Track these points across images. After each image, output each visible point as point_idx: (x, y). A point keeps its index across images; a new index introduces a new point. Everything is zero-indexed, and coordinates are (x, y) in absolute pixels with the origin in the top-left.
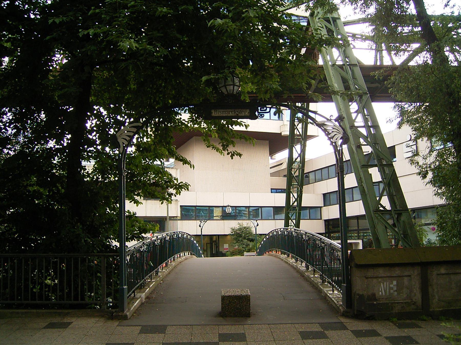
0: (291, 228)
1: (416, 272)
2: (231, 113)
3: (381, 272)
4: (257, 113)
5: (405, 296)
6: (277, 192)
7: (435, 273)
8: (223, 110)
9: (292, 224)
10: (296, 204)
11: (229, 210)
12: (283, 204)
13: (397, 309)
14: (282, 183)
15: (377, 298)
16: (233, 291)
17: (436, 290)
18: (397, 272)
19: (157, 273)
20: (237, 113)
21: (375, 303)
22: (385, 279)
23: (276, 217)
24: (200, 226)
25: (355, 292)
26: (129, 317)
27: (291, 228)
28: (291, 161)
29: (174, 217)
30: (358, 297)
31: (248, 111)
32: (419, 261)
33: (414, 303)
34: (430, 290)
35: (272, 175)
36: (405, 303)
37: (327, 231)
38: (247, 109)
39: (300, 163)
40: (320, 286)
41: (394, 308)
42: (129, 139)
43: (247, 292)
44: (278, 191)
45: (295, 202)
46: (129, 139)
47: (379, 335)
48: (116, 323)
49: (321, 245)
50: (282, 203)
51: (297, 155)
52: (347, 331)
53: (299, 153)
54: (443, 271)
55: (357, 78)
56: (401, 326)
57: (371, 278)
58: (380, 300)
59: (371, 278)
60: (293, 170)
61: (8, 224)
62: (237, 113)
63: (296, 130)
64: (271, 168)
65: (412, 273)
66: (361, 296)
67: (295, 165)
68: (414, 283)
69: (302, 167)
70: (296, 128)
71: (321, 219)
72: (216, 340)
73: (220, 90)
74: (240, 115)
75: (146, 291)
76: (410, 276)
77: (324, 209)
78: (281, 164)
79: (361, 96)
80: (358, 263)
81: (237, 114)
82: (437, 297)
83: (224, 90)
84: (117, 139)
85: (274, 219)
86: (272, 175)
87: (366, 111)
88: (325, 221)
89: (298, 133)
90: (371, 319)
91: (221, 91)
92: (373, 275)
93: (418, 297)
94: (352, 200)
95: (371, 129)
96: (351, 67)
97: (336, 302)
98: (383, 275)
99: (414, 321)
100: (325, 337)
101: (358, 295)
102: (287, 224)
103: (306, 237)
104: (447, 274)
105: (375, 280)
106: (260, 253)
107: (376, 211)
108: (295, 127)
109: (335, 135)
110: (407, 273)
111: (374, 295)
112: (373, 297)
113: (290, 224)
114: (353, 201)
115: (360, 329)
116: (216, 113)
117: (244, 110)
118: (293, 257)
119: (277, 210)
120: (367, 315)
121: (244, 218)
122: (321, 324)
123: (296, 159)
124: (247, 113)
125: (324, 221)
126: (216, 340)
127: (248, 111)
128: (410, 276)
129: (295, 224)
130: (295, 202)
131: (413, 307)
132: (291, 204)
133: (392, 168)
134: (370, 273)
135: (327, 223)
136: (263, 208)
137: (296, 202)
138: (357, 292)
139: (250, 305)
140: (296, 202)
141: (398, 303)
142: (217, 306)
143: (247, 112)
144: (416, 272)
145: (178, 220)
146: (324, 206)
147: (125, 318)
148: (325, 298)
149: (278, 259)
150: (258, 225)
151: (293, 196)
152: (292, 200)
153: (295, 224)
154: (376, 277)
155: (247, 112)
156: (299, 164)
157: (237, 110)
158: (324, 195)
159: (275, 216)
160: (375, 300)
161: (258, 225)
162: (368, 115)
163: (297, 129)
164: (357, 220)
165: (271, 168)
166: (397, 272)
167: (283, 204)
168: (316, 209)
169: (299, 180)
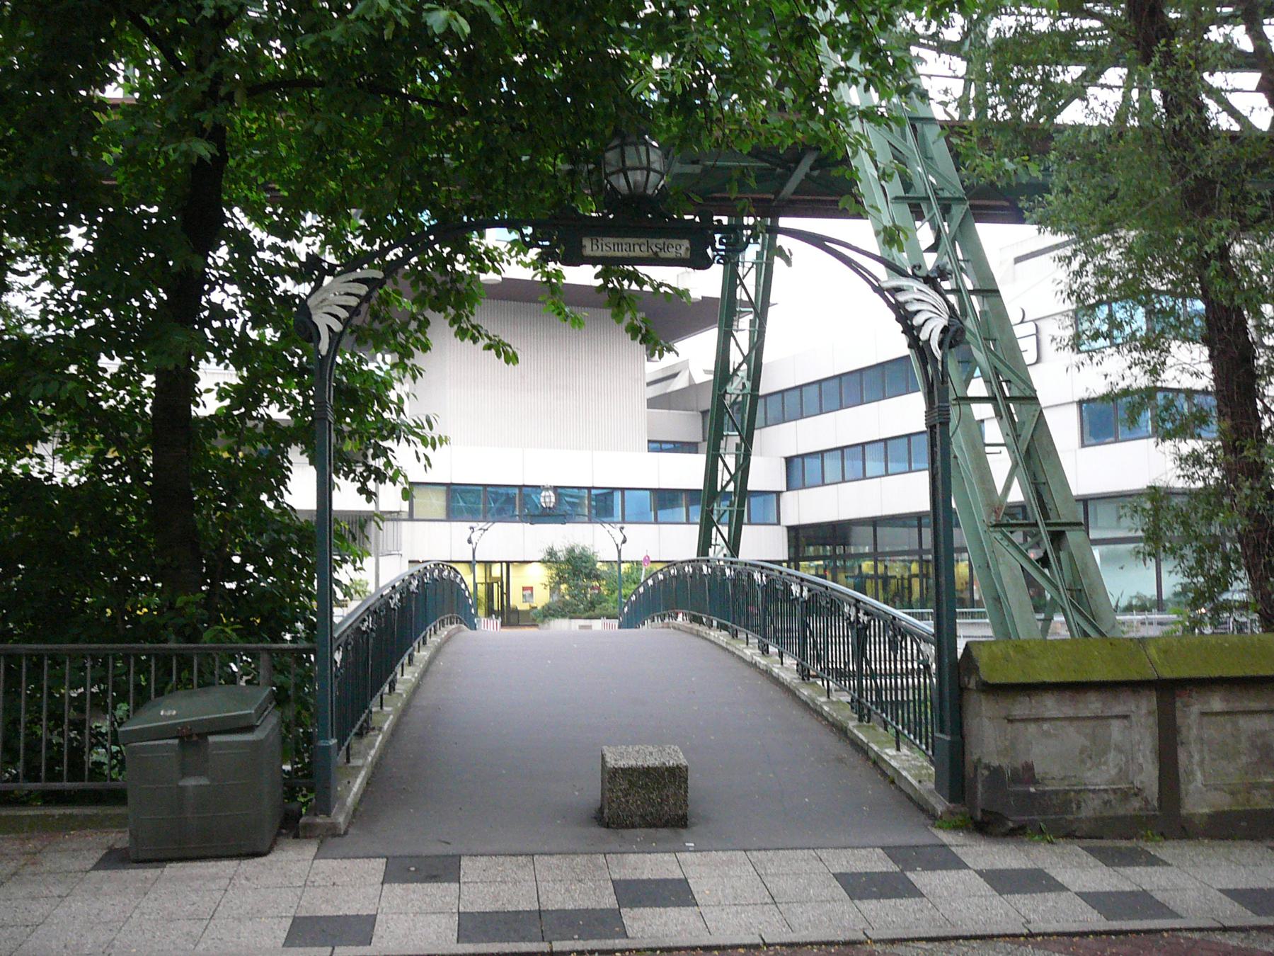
0: (718, 551)
1: (1143, 708)
2: (637, 247)
3: (1050, 705)
4: (709, 251)
5: (1113, 772)
6: (661, 450)
7: (1195, 709)
8: (615, 240)
9: (720, 540)
10: (731, 488)
11: (548, 499)
12: (698, 483)
13: (1090, 808)
14: (686, 425)
15: (1037, 776)
16: (638, 752)
17: (1197, 758)
18: (1092, 706)
19: (392, 688)
20: (655, 249)
21: (1032, 790)
22: (1058, 723)
23: (662, 514)
24: (470, 541)
25: (979, 760)
26: (343, 827)
27: (718, 551)
28: (723, 373)
29: (391, 512)
30: (986, 773)
31: (686, 244)
32: (1154, 677)
33: (1138, 792)
34: (1182, 756)
35: (653, 403)
36: (1114, 791)
37: (792, 556)
38: (684, 238)
39: (748, 379)
40: (855, 731)
41: (1083, 804)
42: (347, 315)
43: (673, 756)
44: (664, 446)
45: (728, 483)
46: (347, 315)
47: (1061, 888)
48: (311, 849)
49: (858, 618)
50: (696, 481)
51: (741, 359)
52: (966, 871)
53: (746, 352)
54: (1217, 704)
55: (936, 156)
56: (1111, 858)
57: (1022, 720)
58: (1046, 782)
59: (1022, 720)
60: (728, 397)
61: (109, 617)
62: (655, 249)
63: (739, 289)
64: (649, 384)
65: (1133, 708)
66: (996, 772)
67: (734, 387)
68: (1137, 737)
69: (752, 390)
70: (742, 283)
71: (779, 523)
72: (609, 901)
73: (609, 182)
74: (662, 255)
75: (377, 744)
76: (1126, 717)
77: (788, 498)
78: (675, 375)
79: (946, 210)
80: (991, 682)
81: (656, 253)
82: (1199, 775)
83: (620, 183)
84: (310, 316)
85: (656, 522)
86: (653, 403)
87: (961, 250)
88: (791, 529)
89: (745, 298)
90: (1016, 833)
91: (611, 185)
92: (1027, 712)
93: (1148, 776)
94: (861, 476)
95: (974, 298)
96: (918, 125)
97: (914, 782)
98: (1054, 713)
99: (1142, 844)
100: (913, 892)
101: (987, 767)
102: (705, 543)
103: (802, 590)
104: (1228, 713)
105: (1032, 728)
106: (631, 620)
107: (995, 526)
108: (738, 282)
109: (926, 321)
110: (1119, 709)
111: (1029, 768)
112: (1027, 774)
113: (713, 542)
114: (865, 478)
115: (1000, 865)
116: (595, 247)
117: (675, 242)
118: (721, 627)
119: (665, 499)
120: (1011, 824)
121: (582, 518)
122: (891, 852)
123: (736, 371)
124: (682, 247)
125: (785, 530)
126: (609, 901)
127: (686, 244)
128: (1126, 717)
129: (726, 537)
130: (728, 483)
131: (1136, 803)
132: (719, 488)
133: (1034, 407)
134: (1022, 707)
135: (793, 534)
136: (626, 492)
137: (732, 484)
138: (985, 761)
139: (686, 792)
140: (732, 484)
141: (1094, 791)
142: (590, 791)
143: (683, 248)
144: (1143, 708)
145: (404, 520)
146: (788, 489)
147: (332, 832)
148: (891, 779)
149: (704, 643)
150: (624, 541)
151: (725, 465)
152: (723, 477)
153: (726, 537)
154: (1036, 720)
155: (683, 248)
156: (745, 380)
157: (655, 241)
158: (789, 461)
159: (659, 512)
160: (1033, 780)
161: (624, 541)
162: (968, 261)
163: (744, 287)
164: (872, 529)
165: (649, 384)
166: (1093, 704)
167: (698, 483)
168: (767, 497)
169: (742, 423)
